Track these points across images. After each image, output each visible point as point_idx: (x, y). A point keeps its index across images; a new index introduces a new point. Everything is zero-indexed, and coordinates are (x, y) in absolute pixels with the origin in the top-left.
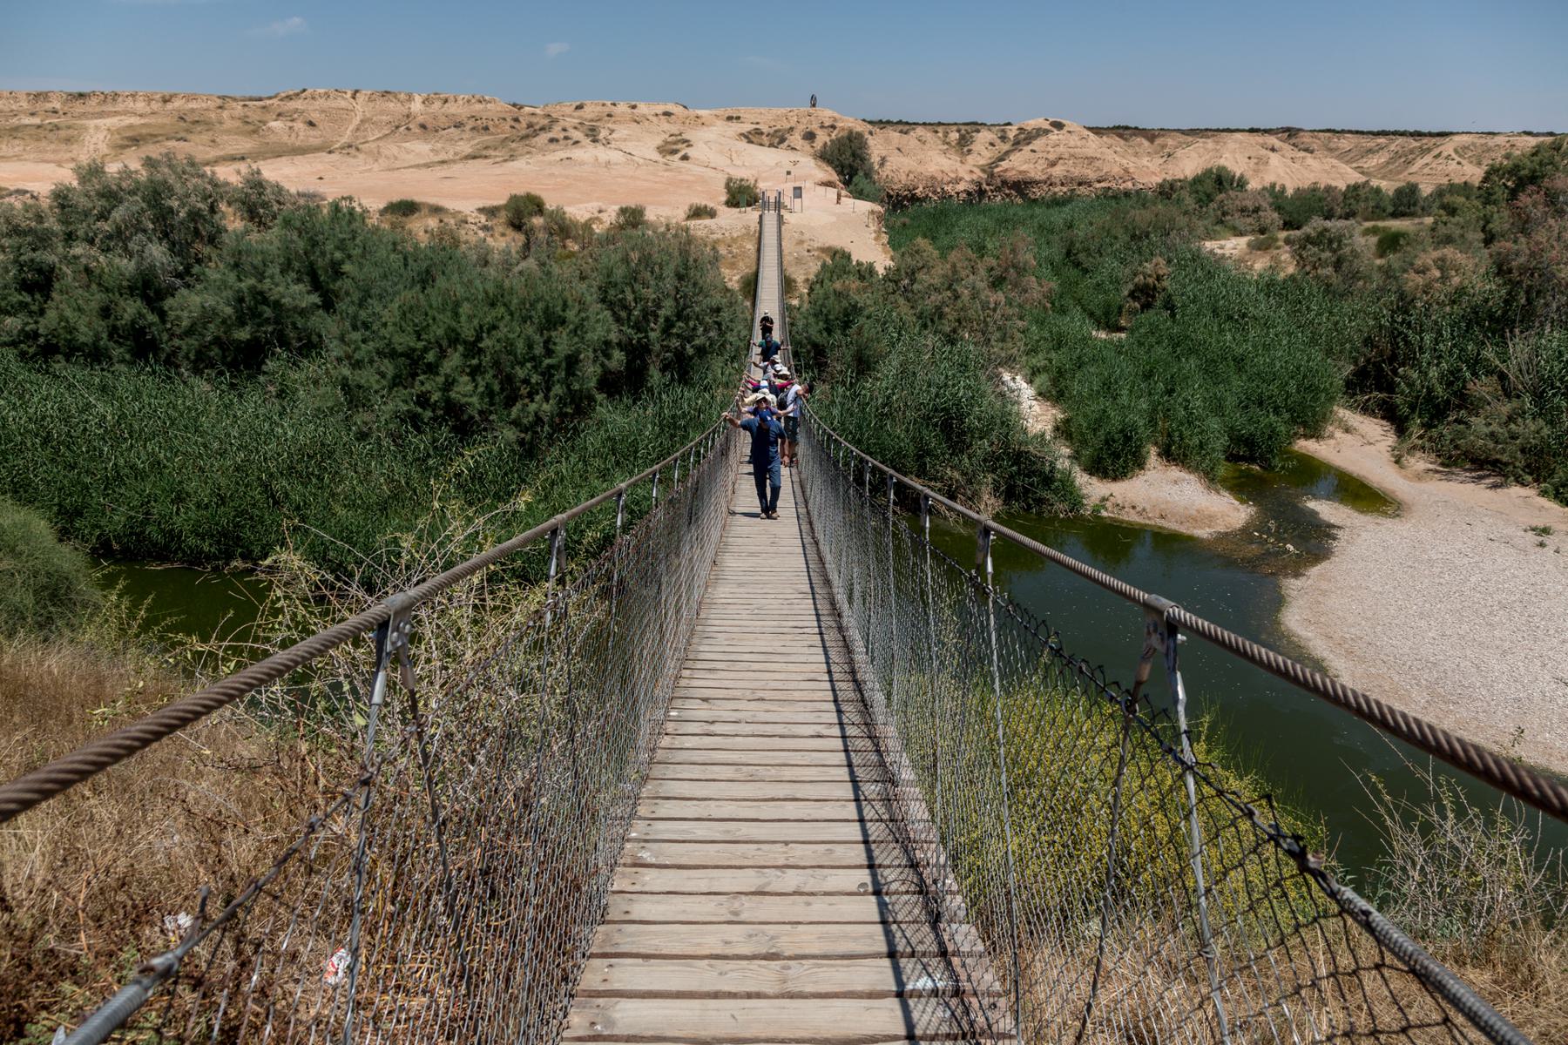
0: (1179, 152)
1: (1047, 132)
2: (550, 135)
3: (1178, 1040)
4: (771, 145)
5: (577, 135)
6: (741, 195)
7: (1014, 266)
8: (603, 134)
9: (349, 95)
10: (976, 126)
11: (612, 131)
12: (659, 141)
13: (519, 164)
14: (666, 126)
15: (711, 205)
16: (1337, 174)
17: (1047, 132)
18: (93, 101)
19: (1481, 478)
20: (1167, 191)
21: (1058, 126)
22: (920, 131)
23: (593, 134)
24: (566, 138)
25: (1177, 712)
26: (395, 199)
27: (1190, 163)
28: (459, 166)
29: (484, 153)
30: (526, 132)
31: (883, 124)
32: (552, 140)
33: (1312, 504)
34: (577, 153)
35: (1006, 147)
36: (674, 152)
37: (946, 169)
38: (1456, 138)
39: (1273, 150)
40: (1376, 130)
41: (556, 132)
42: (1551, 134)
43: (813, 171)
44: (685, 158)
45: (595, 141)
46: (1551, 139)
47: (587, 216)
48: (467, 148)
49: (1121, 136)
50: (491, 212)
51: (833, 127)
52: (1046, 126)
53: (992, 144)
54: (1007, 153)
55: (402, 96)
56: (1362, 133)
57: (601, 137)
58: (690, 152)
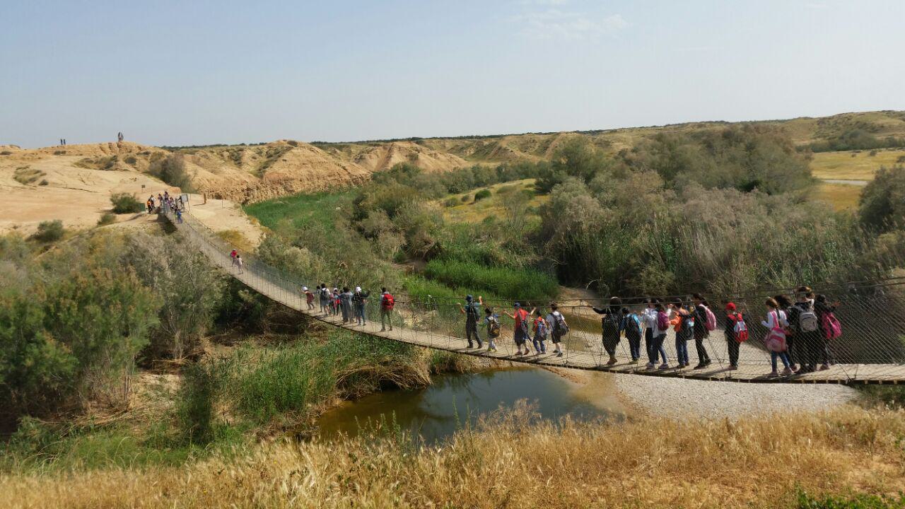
4: (102, 169)
21: (294, 144)
22: (201, 152)
27: (374, 162)
35: (264, 159)
36: (33, 180)
38: (507, 138)
44: (44, 183)
53: (254, 158)
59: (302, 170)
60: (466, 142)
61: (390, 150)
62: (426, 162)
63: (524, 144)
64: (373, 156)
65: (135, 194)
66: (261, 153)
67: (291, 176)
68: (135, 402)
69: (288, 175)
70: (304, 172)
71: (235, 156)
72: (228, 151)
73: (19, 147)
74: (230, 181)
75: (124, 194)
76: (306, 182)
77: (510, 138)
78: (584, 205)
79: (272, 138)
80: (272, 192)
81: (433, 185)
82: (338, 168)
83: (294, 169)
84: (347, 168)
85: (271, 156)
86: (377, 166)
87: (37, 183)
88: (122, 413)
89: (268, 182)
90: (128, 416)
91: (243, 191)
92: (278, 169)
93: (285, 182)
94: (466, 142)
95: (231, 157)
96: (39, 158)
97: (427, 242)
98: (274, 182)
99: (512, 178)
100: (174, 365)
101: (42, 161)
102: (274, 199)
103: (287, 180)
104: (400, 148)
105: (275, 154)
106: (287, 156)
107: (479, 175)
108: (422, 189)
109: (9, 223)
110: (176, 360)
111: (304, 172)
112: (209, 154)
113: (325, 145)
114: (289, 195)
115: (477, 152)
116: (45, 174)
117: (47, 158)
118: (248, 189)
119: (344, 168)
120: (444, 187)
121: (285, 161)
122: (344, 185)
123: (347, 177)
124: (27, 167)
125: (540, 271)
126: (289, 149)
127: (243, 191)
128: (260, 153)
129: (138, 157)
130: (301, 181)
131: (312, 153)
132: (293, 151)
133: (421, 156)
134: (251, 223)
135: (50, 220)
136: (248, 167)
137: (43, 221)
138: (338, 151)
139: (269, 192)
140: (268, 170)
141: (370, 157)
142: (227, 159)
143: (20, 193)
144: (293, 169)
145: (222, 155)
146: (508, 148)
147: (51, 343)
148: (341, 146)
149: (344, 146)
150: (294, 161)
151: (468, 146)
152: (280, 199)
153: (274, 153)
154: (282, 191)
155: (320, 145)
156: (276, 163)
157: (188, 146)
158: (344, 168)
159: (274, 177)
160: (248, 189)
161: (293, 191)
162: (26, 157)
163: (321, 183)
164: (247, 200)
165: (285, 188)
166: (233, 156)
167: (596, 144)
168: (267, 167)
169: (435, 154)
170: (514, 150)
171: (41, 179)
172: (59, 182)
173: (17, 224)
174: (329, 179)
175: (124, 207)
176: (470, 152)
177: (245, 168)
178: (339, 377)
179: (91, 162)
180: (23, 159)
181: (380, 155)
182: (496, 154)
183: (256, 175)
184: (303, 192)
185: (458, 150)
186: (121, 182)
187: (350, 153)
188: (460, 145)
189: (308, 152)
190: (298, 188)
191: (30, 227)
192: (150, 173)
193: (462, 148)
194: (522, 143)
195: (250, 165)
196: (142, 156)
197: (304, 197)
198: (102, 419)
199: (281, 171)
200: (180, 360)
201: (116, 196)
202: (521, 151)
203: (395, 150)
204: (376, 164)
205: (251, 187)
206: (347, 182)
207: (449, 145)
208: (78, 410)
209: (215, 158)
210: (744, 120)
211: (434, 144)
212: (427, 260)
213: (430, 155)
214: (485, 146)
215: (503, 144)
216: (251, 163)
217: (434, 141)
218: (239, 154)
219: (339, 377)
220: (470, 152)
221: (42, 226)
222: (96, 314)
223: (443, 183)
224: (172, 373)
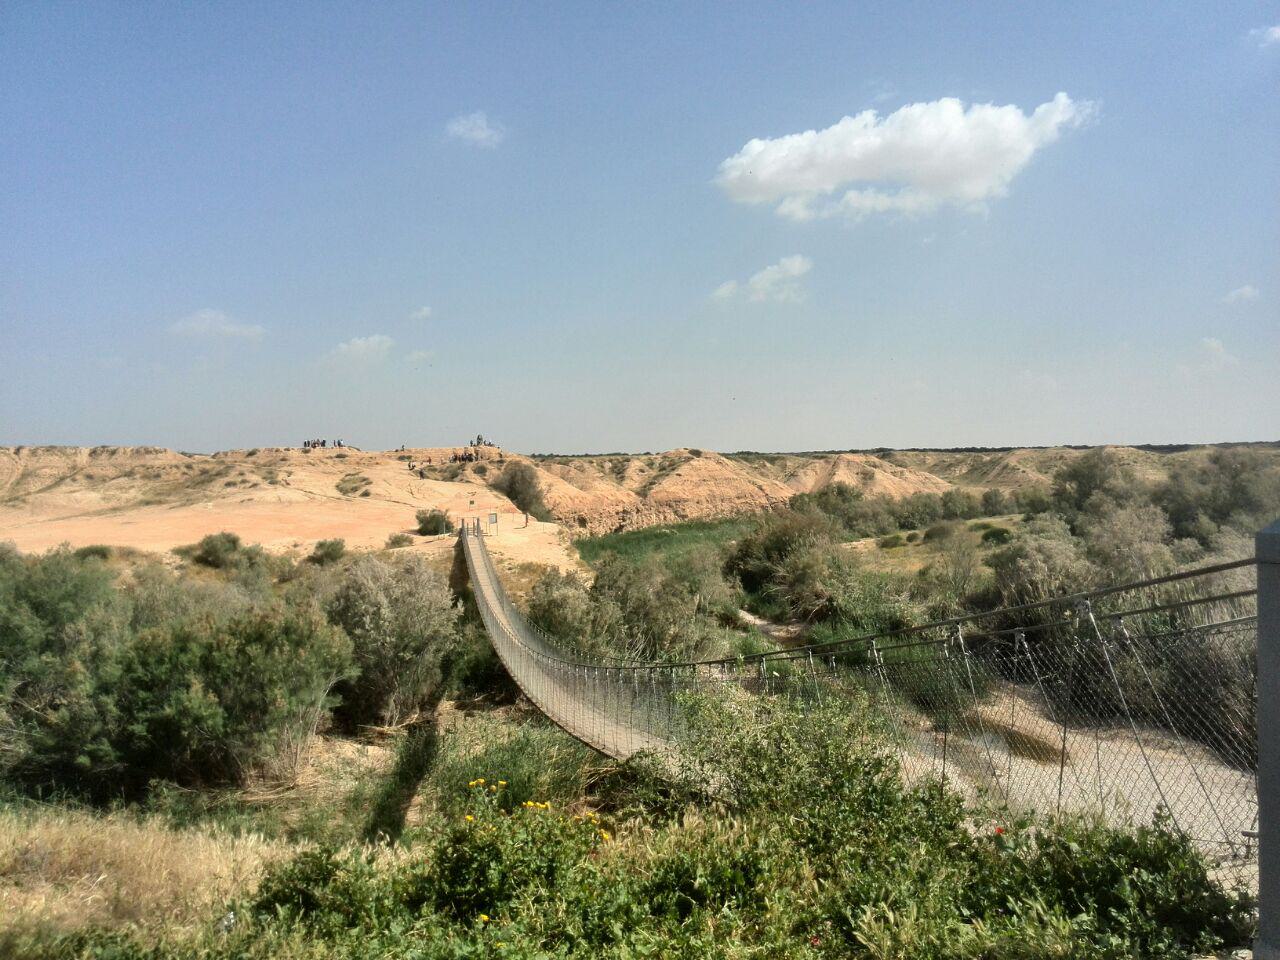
0: (801, 472)
4: (444, 479)
6: (432, 525)
7: (249, 641)
8: (282, 476)
9: (12, 450)
11: (290, 474)
12: (337, 480)
14: (341, 467)
16: (939, 486)
19: (1116, 735)
20: (796, 502)
21: (697, 453)
22: (577, 462)
24: (244, 482)
27: (810, 481)
28: (133, 513)
30: (202, 478)
31: (543, 459)
32: (228, 484)
33: (1060, 109)
34: (256, 494)
35: (654, 473)
36: (355, 490)
37: (606, 494)
38: (1018, 452)
39: (875, 466)
40: (950, 448)
41: (232, 477)
42: (1085, 447)
44: (366, 494)
46: (1083, 452)
47: (283, 551)
48: (134, 494)
49: (746, 460)
50: (183, 552)
51: (501, 462)
53: (642, 471)
55: (69, 451)
56: (940, 451)
57: (280, 478)
58: (371, 488)
59: (700, 489)
60: (957, 456)
61: (835, 465)
62: (886, 483)
63: (1045, 462)
64: (809, 472)
65: (447, 511)
66: (652, 464)
67: (685, 497)
68: (305, 777)
69: (681, 494)
70: (703, 491)
71: (618, 468)
72: (611, 461)
73: (358, 450)
74: (600, 500)
75: (434, 511)
76: (705, 505)
77: (1023, 452)
78: (1055, 554)
79: (670, 448)
80: (657, 516)
81: (875, 515)
82: (751, 487)
83: (691, 487)
84: (764, 488)
85: (664, 469)
86: (814, 486)
87: (360, 492)
88: (283, 791)
89: (654, 504)
90: (292, 794)
91: (617, 513)
92: (669, 486)
93: (674, 504)
94: (957, 456)
95: (612, 470)
96: (377, 464)
97: (818, 596)
98: (660, 503)
99: (1006, 511)
100: (382, 735)
101: (379, 467)
102: (658, 526)
103: (678, 501)
104: (849, 462)
105: (669, 466)
106: (684, 469)
107: (950, 504)
108: (857, 520)
109: (290, 540)
110: (386, 728)
111: (703, 491)
112: (586, 465)
113: (750, 457)
114: (680, 521)
115: (970, 472)
116: (371, 483)
117: (387, 464)
118: (624, 512)
119: (760, 488)
120: (892, 519)
121: (680, 475)
122: (758, 511)
123: (764, 501)
124: (357, 474)
125: (337, 624)
126: (688, 460)
127: (617, 513)
128: (651, 465)
129: (489, 467)
130: (698, 503)
131: (718, 467)
132: (692, 462)
133: (879, 474)
134: (568, 555)
135: (330, 539)
136: (632, 483)
137: (322, 540)
138: (768, 465)
139: (654, 517)
140: (656, 488)
141: (805, 473)
142: (607, 471)
143: (333, 504)
144: (688, 487)
145: (602, 467)
146: (1019, 466)
147: (197, 685)
148: (772, 459)
149: (776, 459)
150: (692, 476)
151: (959, 462)
152: (667, 526)
153: (669, 466)
154: (672, 517)
155: (745, 456)
156: (667, 479)
157: (580, 454)
158: (760, 488)
159: (662, 496)
160: (624, 512)
161: (686, 516)
162: (363, 461)
163: (726, 506)
164: (621, 527)
165: (676, 512)
166: (616, 467)
167: (1164, 465)
168: (654, 483)
169: (902, 472)
170: (1028, 470)
171: (364, 489)
172: (384, 493)
173: (299, 542)
174: (737, 501)
175: (431, 527)
176: (960, 471)
177: (628, 483)
178: (591, 776)
179: (435, 470)
180: (358, 463)
181: (818, 471)
182: (999, 474)
183: (638, 493)
184: (699, 518)
185: (941, 469)
186: (456, 496)
187: (784, 467)
188: (946, 459)
189: (712, 464)
190: (692, 512)
191: (308, 549)
192: (495, 486)
193: (951, 465)
194: (1041, 459)
195: (635, 478)
196: (496, 465)
197: (700, 525)
198: (257, 794)
199: (672, 489)
200: (393, 727)
201: (424, 512)
202: (1040, 472)
203: (842, 465)
204: (813, 483)
205: (628, 508)
206: (762, 507)
207: (930, 459)
208: (236, 781)
209: (592, 471)
210: (1226, 441)
211: (909, 458)
212: (811, 622)
213: (894, 474)
214: (982, 461)
215: (1012, 461)
216: (636, 478)
217: (909, 453)
218: (623, 466)
219: (591, 776)
220: (960, 471)
221: (321, 545)
222: (256, 658)
223: (892, 513)
224: (379, 745)
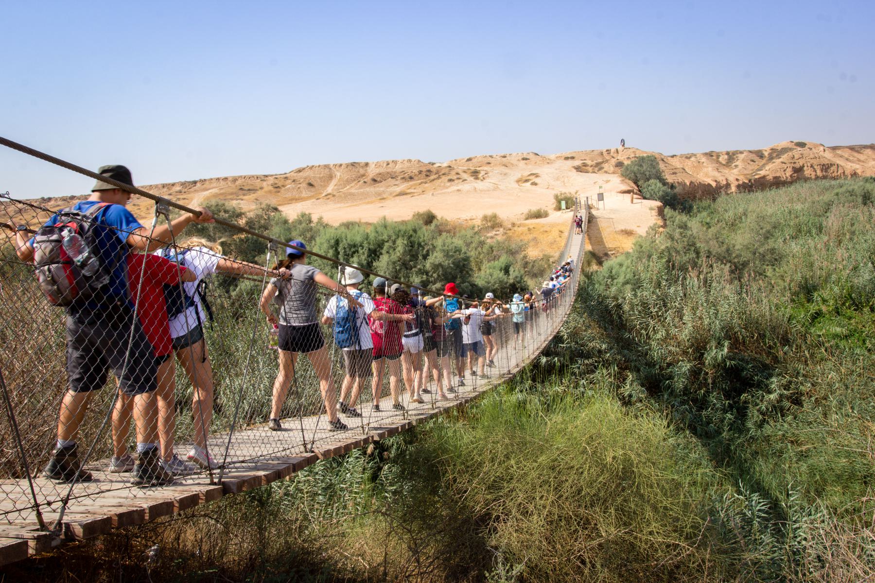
1: (791, 149)
2: (449, 177)
3: (873, 553)
5: (465, 176)
10: (735, 153)
13: (428, 196)
15: (544, 208)
17: (791, 149)
18: (198, 185)
23: (475, 174)
24: (459, 179)
25: (275, 414)
26: (345, 221)
29: (409, 191)
32: (450, 180)
43: (615, 182)
44: (534, 184)
45: (477, 178)
48: (398, 189)
52: (791, 146)
54: (764, 165)
